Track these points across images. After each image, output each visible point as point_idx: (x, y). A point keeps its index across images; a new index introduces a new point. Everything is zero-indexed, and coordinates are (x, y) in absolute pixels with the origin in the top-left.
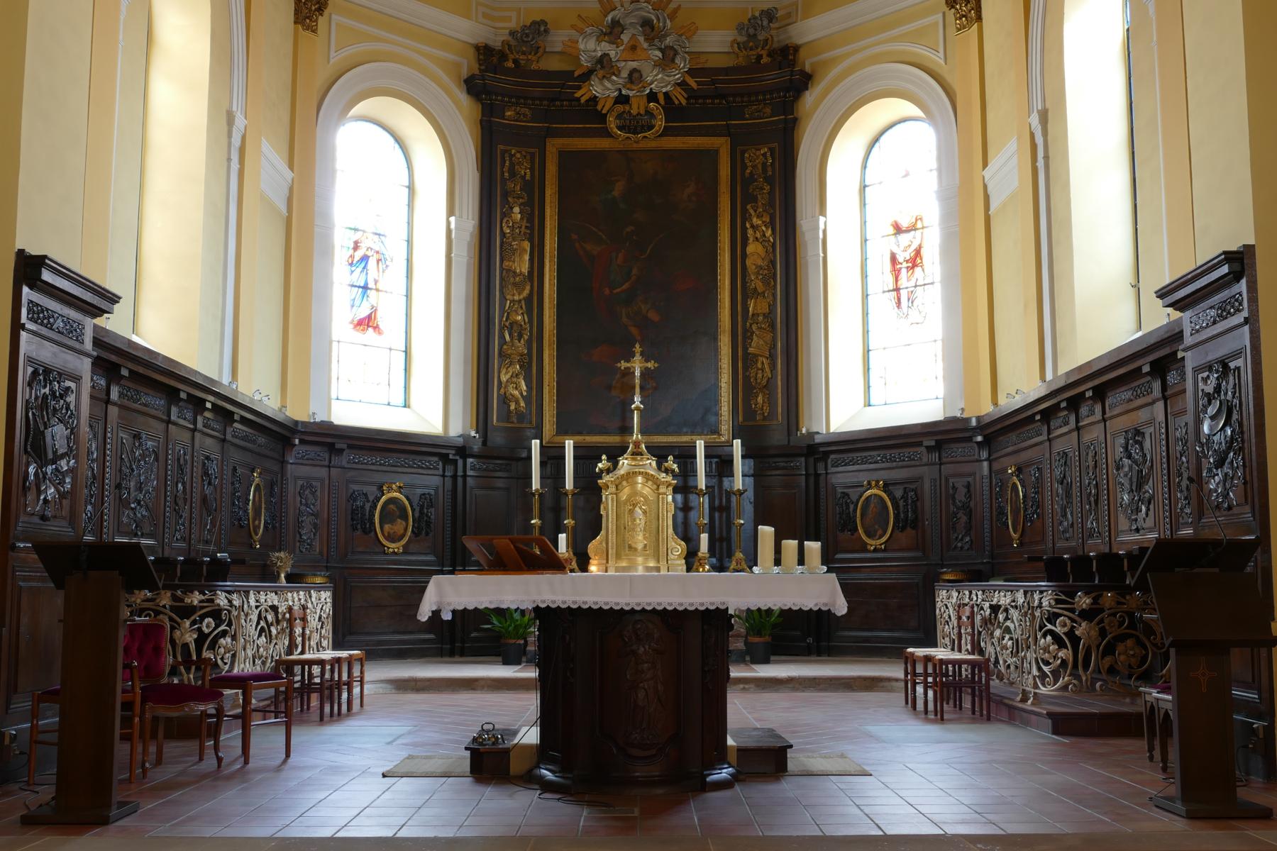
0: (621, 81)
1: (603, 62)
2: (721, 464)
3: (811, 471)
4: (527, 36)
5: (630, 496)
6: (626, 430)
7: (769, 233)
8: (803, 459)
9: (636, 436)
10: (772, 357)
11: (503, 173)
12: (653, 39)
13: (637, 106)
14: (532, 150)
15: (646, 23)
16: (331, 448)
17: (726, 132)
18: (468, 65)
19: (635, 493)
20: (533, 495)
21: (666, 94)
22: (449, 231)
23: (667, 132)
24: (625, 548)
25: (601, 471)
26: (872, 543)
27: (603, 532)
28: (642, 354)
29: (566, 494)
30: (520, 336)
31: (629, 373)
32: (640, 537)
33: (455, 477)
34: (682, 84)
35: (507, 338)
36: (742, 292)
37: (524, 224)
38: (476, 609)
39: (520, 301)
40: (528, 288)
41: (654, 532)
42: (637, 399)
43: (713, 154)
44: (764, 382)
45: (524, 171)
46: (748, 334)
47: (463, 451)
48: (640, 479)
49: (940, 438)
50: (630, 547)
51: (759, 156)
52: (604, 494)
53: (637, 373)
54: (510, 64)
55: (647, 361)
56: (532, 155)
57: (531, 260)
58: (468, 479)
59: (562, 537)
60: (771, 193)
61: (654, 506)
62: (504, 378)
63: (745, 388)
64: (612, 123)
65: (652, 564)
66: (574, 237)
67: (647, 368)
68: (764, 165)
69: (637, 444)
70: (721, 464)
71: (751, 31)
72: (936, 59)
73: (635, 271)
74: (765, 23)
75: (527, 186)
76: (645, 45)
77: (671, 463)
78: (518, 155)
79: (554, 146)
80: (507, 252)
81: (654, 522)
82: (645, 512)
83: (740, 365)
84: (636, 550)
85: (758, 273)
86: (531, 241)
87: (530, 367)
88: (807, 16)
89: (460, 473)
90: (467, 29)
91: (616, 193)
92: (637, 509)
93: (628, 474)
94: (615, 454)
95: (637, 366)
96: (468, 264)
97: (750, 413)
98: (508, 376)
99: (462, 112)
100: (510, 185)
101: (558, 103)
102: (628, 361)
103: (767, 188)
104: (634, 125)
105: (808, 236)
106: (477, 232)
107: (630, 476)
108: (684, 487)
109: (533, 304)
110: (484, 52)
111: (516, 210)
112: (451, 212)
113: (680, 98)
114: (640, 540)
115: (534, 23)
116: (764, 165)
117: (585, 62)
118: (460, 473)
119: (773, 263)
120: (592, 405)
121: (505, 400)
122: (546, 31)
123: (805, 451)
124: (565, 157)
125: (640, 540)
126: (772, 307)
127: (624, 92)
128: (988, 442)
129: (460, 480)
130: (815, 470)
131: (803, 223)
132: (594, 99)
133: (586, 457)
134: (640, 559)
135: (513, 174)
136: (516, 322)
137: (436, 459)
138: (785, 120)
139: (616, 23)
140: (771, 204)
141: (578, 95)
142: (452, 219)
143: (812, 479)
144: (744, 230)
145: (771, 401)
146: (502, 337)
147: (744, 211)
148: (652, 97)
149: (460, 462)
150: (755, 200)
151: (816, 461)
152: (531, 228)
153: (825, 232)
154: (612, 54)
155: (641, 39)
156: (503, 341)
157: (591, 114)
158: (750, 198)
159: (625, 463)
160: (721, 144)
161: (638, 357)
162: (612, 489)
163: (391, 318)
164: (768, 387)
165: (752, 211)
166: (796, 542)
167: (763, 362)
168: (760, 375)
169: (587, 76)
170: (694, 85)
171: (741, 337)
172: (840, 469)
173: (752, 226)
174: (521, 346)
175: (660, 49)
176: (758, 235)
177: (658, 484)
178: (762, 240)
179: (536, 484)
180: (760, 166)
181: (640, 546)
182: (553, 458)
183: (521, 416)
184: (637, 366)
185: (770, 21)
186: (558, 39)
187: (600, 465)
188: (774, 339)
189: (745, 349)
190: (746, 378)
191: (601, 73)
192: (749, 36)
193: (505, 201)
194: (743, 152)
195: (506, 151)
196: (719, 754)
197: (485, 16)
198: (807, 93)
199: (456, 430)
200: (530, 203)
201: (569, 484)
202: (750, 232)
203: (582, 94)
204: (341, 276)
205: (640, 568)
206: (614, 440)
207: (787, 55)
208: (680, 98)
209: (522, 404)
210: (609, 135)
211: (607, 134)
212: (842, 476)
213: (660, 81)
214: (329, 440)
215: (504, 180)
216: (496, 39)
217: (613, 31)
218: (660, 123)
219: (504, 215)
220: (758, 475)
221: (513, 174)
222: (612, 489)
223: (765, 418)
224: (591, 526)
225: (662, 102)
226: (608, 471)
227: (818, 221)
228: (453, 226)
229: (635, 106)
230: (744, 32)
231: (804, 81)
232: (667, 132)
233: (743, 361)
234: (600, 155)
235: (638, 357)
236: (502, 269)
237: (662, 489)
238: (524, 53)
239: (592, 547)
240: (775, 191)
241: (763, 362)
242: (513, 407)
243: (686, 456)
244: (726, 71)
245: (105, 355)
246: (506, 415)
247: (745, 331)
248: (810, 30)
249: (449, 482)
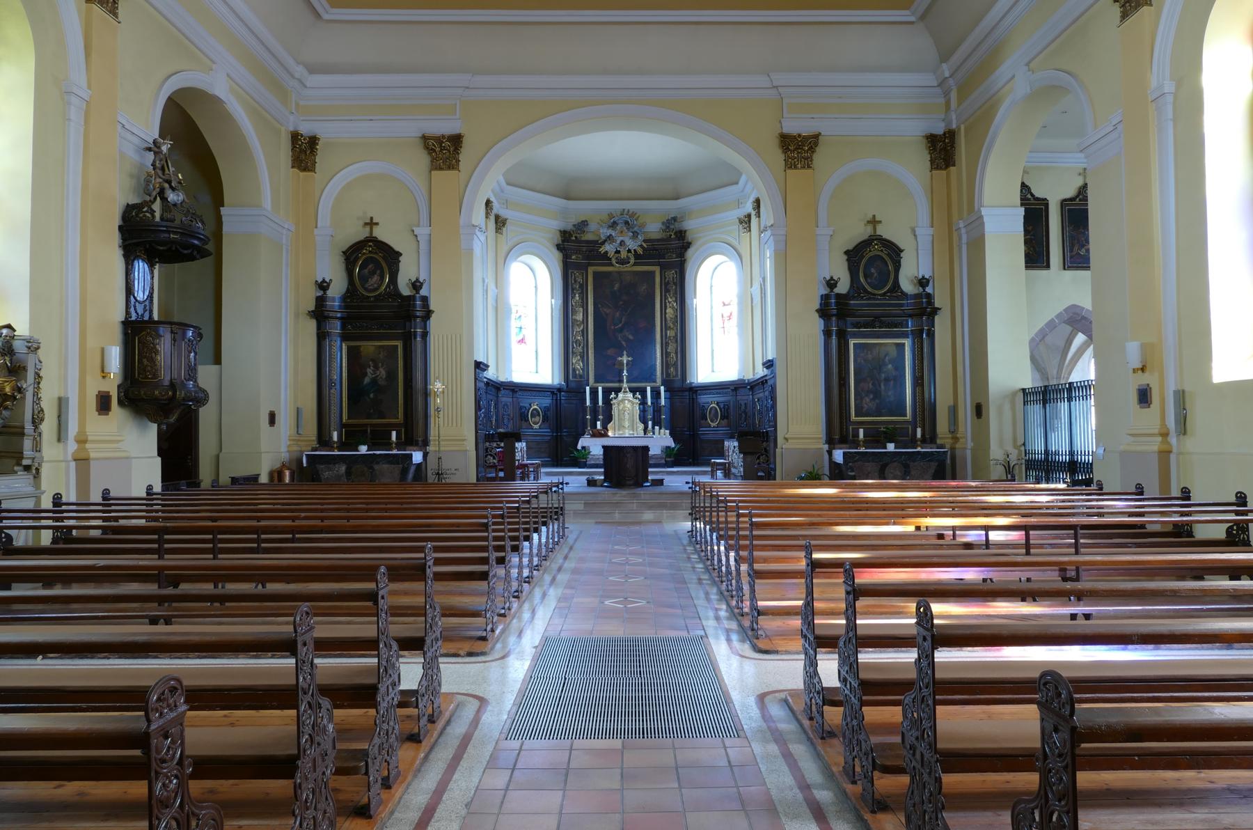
1: (610, 238)
2: (656, 394)
6: (621, 381)
9: (625, 385)
13: (624, 254)
15: (626, 223)
16: (513, 391)
18: (558, 239)
23: (635, 264)
24: (621, 427)
26: (713, 424)
34: (641, 246)
36: (665, 327)
38: (161, 453)
43: (653, 273)
46: (667, 344)
47: (560, 390)
49: (735, 387)
51: (671, 274)
64: (614, 261)
70: (656, 394)
72: (735, 243)
75: (581, 286)
77: (638, 395)
79: (591, 270)
80: (574, 312)
87: (584, 357)
94: (618, 391)
95: (625, 359)
97: (668, 375)
99: (556, 256)
104: (623, 262)
107: (623, 401)
108: (643, 402)
109: (584, 333)
113: (640, 251)
114: (627, 424)
117: (603, 238)
121: (574, 370)
124: (596, 274)
125: (627, 424)
128: (752, 388)
131: (688, 301)
133: (607, 392)
139: (615, 223)
145: (676, 370)
148: (629, 251)
157: (605, 256)
158: (667, 291)
159: (621, 395)
160: (657, 269)
163: (530, 339)
167: (673, 355)
169: (603, 243)
171: (664, 345)
174: (580, 349)
178: (673, 307)
179: (588, 403)
182: (594, 392)
183: (581, 376)
184: (625, 359)
186: (593, 227)
196: (647, 481)
199: (836, 656)
203: (602, 250)
204: (514, 324)
206: (616, 385)
207: (681, 234)
208: (640, 251)
211: (612, 265)
212: (704, 399)
213: (632, 244)
214: (803, 543)
216: (569, 227)
217: (613, 225)
218: (632, 261)
220: (670, 399)
224: (608, 418)
231: (688, 245)
232: (635, 264)
233: (665, 354)
234: (610, 273)
239: (609, 426)
240: (678, 288)
241: (673, 355)
243: (643, 392)
244: (658, 240)
246: (575, 375)
248: (690, 225)
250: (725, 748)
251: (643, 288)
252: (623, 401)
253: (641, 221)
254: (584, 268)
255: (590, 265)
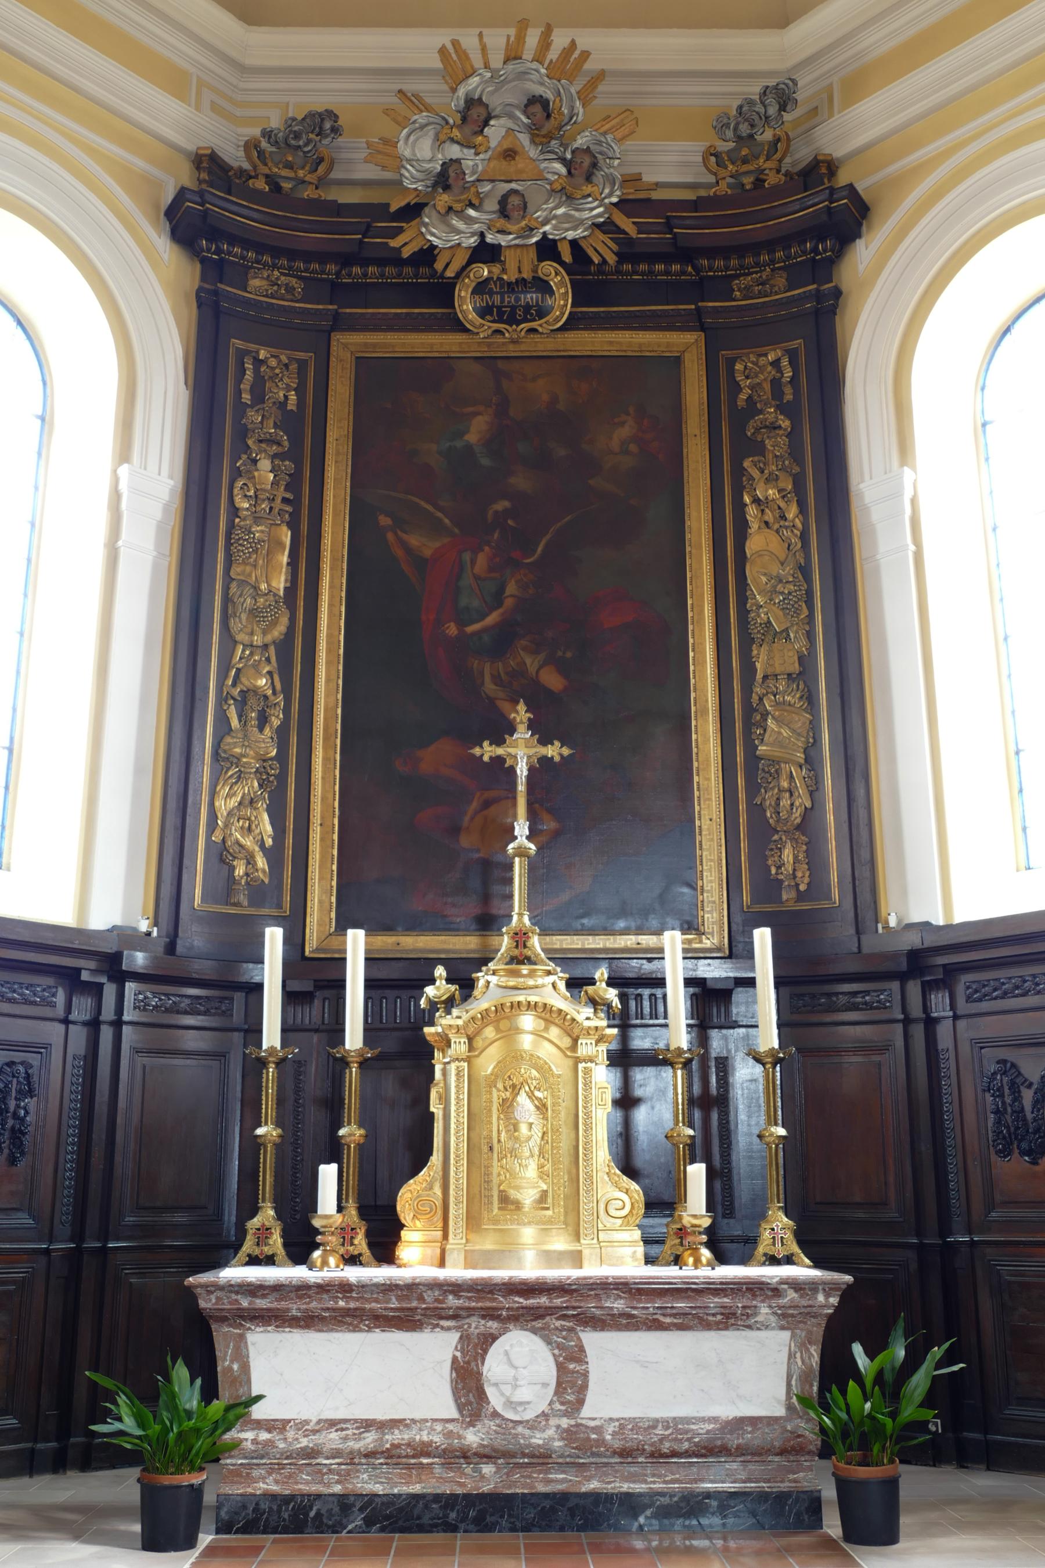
0: (485, 217)
3: (916, 1011)
4: (297, 136)
5: (501, 1065)
7: (792, 512)
8: (895, 986)
10: (811, 761)
11: (239, 393)
12: (550, 137)
13: (517, 265)
14: (302, 355)
17: (698, 322)
18: (180, 176)
19: (514, 1057)
20: (263, 1063)
21: (574, 244)
22: (116, 496)
23: (573, 323)
25: (433, 1005)
27: (436, 1159)
28: (531, 725)
29: (344, 1062)
30: (263, 720)
31: (503, 770)
32: (531, 1171)
33: (94, 1025)
34: (606, 227)
35: (235, 722)
37: (281, 493)
39: (265, 646)
40: (284, 621)
41: (566, 1160)
42: (521, 828)
44: (797, 816)
45: (284, 391)
48: (527, 1021)
50: (505, 1199)
51: (761, 367)
52: (439, 1060)
53: (522, 770)
54: (260, 184)
55: (544, 741)
56: (302, 365)
57: (293, 563)
58: (126, 1030)
59: (328, 1174)
60: (794, 435)
61: (565, 1092)
62: (223, 806)
63: (754, 832)
64: (466, 306)
65: (560, 1243)
66: (384, 521)
67: (545, 760)
68: (776, 383)
69: (520, 938)
71: (744, 129)
73: (511, 589)
74: (772, 111)
76: (533, 152)
78: (273, 362)
81: (566, 1132)
82: (541, 1107)
83: (741, 782)
84: (518, 1205)
85: (774, 591)
86: (293, 525)
87: (285, 792)
88: (849, 101)
89: (108, 1012)
90: (180, 123)
91: (472, 437)
92: (522, 1099)
93: (500, 1008)
95: (521, 752)
96: (156, 566)
98: (233, 802)
100: (254, 417)
101: (357, 270)
102: (499, 742)
103: (785, 423)
104: (510, 306)
105: (876, 514)
106: (177, 504)
109: (294, 656)
110: (208, 163)
111: (265, 464)
112: (124, 454)
113: (603, 250)
115: (311, 115)
116: (776, 383)
117: (413, 181)
118: (108, 1012)
119: (805, 570)
120: (419, 854)
121: (222, 855)
122: (336, 130)
123: (904, 966)
124: (367, 369)
125: (529, 1180)
126: (806, 661)
127: (490, 238)
129: (106, 1034)
130: (926, 1008)
132: (428, 254)
134: (528, 1234)
135: (259, 395)
136: (255, 691)
137: (50, 981)
138: (818, 296)
140: (795, 452)
141: (394, 243)
142: (124, 470)
143: (918, 1032)
144: (740, 508)
146: (222, 719)
147: (738, 472)
148: (547, 249)
149: (110, 991)
150: (759, 449)
151: (927, 988)
152: (294, 503)
153: (914, 501)
154: (468, 165)
155: (524, 139)
156: (223, 726)
157: (426, 287)
159: (490, 982)
161: (522, 734)
162: (459, 1046)
164: (808, 826)
165: (755, 473)
166: (124, 1027)
168: (785, 802)
169: (413, 211)
170: (632, 231)
171: (741, 721)
172: (985, 1006)
173: (756, 501)
174: (266, 743)
175: (563, 160)
176: (769, 516)
177: (574, 1033)
180: (767, 386)
181: (528, 1197)
182: (314, 982)
185: (783, 108)
187: (430, 991)
188: (814, 727)
189: (750, 748)
190: (756, 811)
191: (443, 199)
192: (739, 139)
193: (241, 445)
194: (731, 362)
195: (247, 352)
197: (215, 108)
198: (860, 244)
200: (294, 454)
201: (354, 1038)
202: (752, 511)
203: (406, 242)
205: (529, 1255)
206: (466, 943)
208: (603, 250)
209: (261, 862)
210: (459, 327)
213: (569, 221)
215: (240, 409)
218: (561, 302)
219: (236, 473)
221: (259, 395)
222: (459, 1046)
223: (801, 897)
225: (567, 258)
226: (449, 1004)
227: (900, 477)
228: (123, 486)
229: (512, 265)
230: (730, 134)
232: (573, 323)
234: (440, 368)
235: (522, 734)
236: (228, 579)
237: (586, 1047)
238: (289, 166)
239: (409, 1197)
240: (800, 428)
242: (240, 871)
245: (688, 1161)
246: (223, 886)
247: (749, 710)
249: (78, 1036)
250: (599, 1242)
251: (617, 438)
252: (503, 1015)
253: (518, 1182)
254: (318, 338)
255: (338, 323)
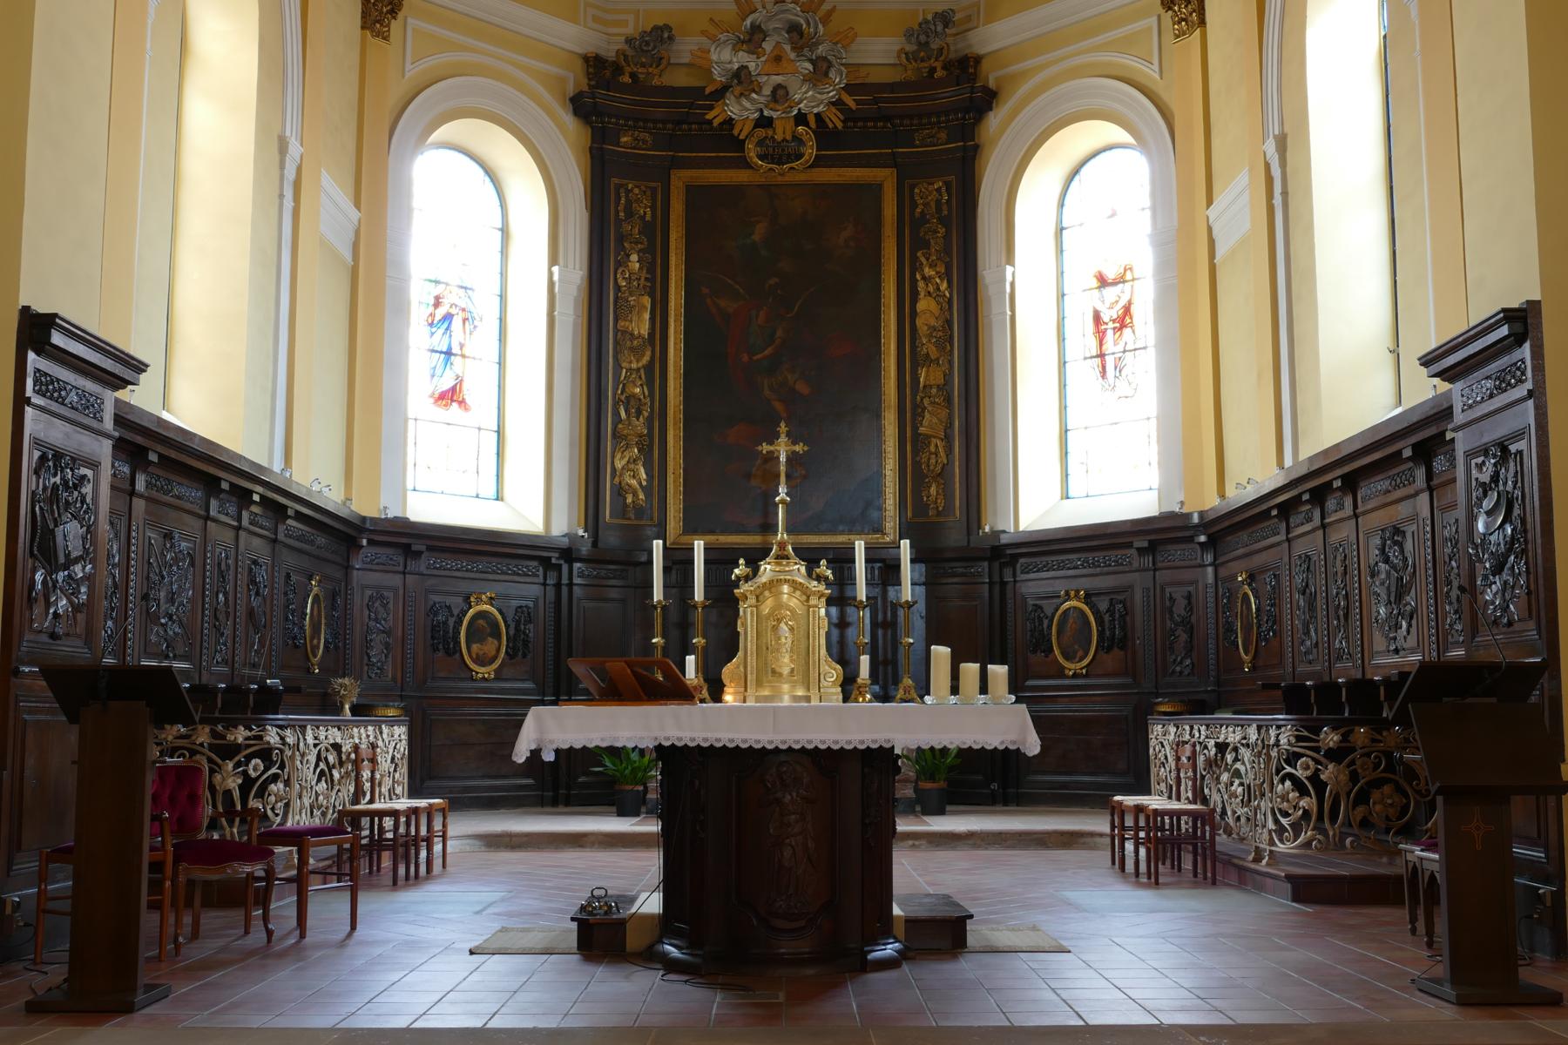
0: (762, 99)
1: (741, 76)
2: (885, 570)
3: (996, 578)
4: (647, 44)
5: (773, 610)
6: (769, 527)
7: (944, 286)
8: (986, 564)
9: (781, 535)
10: (948, 439)
11: (617, 212)
12: (802, 48)
13: (782, 130)
14: (653, 184)
15: (794, 29)
16: (407, 550)
17: (892, 162)
18: (575, 79)
19: (779, 606)
20: (655, 607)
21: (818, 115)
22: (551, 284)
23: (819, 162)
24: (767, 673)
25: (739, 578)
26: (1071, 667)
27: (740, 654)
28: (788, 435)
29: (695, 607)
30: (639, 413)
31: (772, 458)
32: (786, 660)
33: (558, 586)
34: (838, 104)
35: (623, 414)
36: (911, 358)
37: (644, 274)
38: (584, 747)
39: (638, 370)
40: (648, 353)
41: (804, 653)
42: (782, 490)
43: (876, 189)
44: (938, 469)
45: (644, 210)
46: (918, 410)
47: (568, 553)
48: (786, 588)
49: (1154, 538)
50: (774, 672)
51: (932, 192)
52: (742, 607)
53: (783, 458)
54: (626, 79)
55: (794, 443)
56: (654, 190)
57: (652, 319)
58: (575, 588)
59: (690, 660)
60: (947, 237)
61: (803, 622)
62: (619, 465)
63: (915, 476)
64: (752, 151)
65: (800, 693)
66: (705, 290)
67: (794, 452)
68: (938, 202)
69: (782, 545)
70: (885, 570)
71: (923, 38)
72: (1149, 72)
73: (779, 333)
74: (940, 28)
75: (648, 229)
76: (793, 56)
77: (824, 569)
78: (636, 191)
79: (680, 179)
80: (622, 310)
81: (804, 641)
82: (792, 629)
83: (909, 448)
84: (781, 675)
85: (931, 336)
86: (652, 295)
87: (651, 450)
88: (990, 19)
89: (565, 581)
90: (573, 36)
91: (756, 237)
92: (782, 625)
93: (771, 582)
94: (755, 558)
95: (783, 450)
96: (575, 324)
97: (921, 507)
98: (624, 462)
99: (567, 137)
100: (627, 227)
101: (685, 126)
102: (771, 443)
103: (942, 231)
104: (779, 154)
105: (992, 290)
106: (585, 284)
107: (773, 585)
108: (840, 598)
109: (655, 373)
110: (595, 64)
111: (634, 257)
112: (553, 260)
113: (835, 120)
114: (786, 663)
115: (656, 28)
116: (938, 202)
117: (719, 76)
118: (565, 581)
119: (949, 322)
120: (727, 497)
121: (620, 491)
122: (671, 38)
123: (989, 554)
124: (694, 193)
125: (786, 663)
126: (948, 377)
127: (766, 113)
128: (1213, 543)
129: (565, 590)
130: (1001, 577)
131: (986, 274)
132: (729, 122)
133: (719, 561)
134: (786, 687)
135: (630, 213)
136: (634, 395)
137: (535, 563)
138: (964, 148)
139: (756, 29)
140: (947, 250)
141: (709, 116)
142: (556, 269)
143: (997, 589)
144: (914, 282)
145: (947, 492)
146: (616, 413)
147: (914, 259)
148: (801, 119)
149: (565, 568)
150: (927, 245)
151: (1002, 566)
152: (652, 280)
153: (1012, 284)
154: (752, 66)
155: (788, 48)
156: (617, 419)
157: (726, 139)
158: (920, 244)
159: (767, 569)
160: (886, 177)
161: (783, 439)
162: (752, 600)
163: (481, 390)
164: (943, 475)
165: (923, 260)
167: (937, 444)
168: (933, 461)
169: (720, 93)
170: (852, 105)
171: (910, 414)
172: (1032, 576)
173: (924, 278)
174: (640, 425)
175: (811, 61)
176: (931, 289)
177: (807, 594)
178: (936, 295)
179: (658, 594)
180: (933, 204)
181: (786, 671)
182: (678, 562)
183: (639, 511)
184: (783, 450)
185: (946, 26)
186: (685, 48)
187: (737, 571)
188: (951, 416)
189: (915, 428)
190: (917, 465)
191: (738, 90)
192: (920, 44)
193: (620, 246)
194: (912, 187)
195: (621, 186)
196: (882, 926)
197: (596, 19)
198: (991, 114)
199: (560, 528)
200: (650, 249)
201: (699, 594)
202: (921, 284)
203: (715, 115)
204: (419, 339)
205: (786, 697)
206: (753, 540)
207: (967, 67)
208: (835, 120)
209: (642, 496)
210: (748, 165)
211: (746, 164)
212: (1034, 584)
213: (810, 99)
214: (404, 540)
215: (618, 222)
216: (609, 48)
217: (753, 38)
218: (810, 151)
219: (619, 264)
220: (930, 583)
221: (630, 213)
222: (752, 600)
223: (939, 514)
224: (726, 645)
225: (813, 125)
226: (747, 579)
227: (1004, 271)
228: (556, 278)
229: (779, 131)
230: (913, 40)
231: (987, 99)
232: (819, 162)
233: (913, 443)
234: (737, 191)
235: (783, 439)
236: (616, 331)
237: (813, 601)
238: (643, 65)
239: (727, 671)
240: (952, 234)
241: (937, 444)
242: (629, 499)
243: (842, 560)
244: (892, 87)
246: (621, 510)
247: (915, 406)
248: (994, 37)
249: (551, 591)
